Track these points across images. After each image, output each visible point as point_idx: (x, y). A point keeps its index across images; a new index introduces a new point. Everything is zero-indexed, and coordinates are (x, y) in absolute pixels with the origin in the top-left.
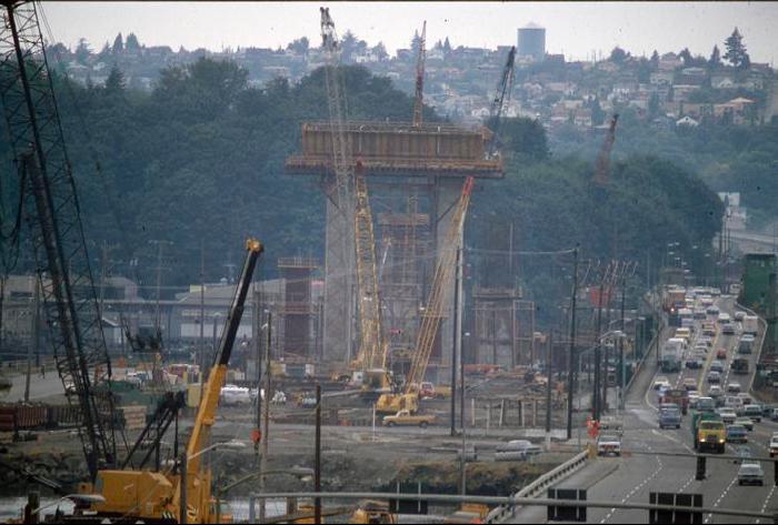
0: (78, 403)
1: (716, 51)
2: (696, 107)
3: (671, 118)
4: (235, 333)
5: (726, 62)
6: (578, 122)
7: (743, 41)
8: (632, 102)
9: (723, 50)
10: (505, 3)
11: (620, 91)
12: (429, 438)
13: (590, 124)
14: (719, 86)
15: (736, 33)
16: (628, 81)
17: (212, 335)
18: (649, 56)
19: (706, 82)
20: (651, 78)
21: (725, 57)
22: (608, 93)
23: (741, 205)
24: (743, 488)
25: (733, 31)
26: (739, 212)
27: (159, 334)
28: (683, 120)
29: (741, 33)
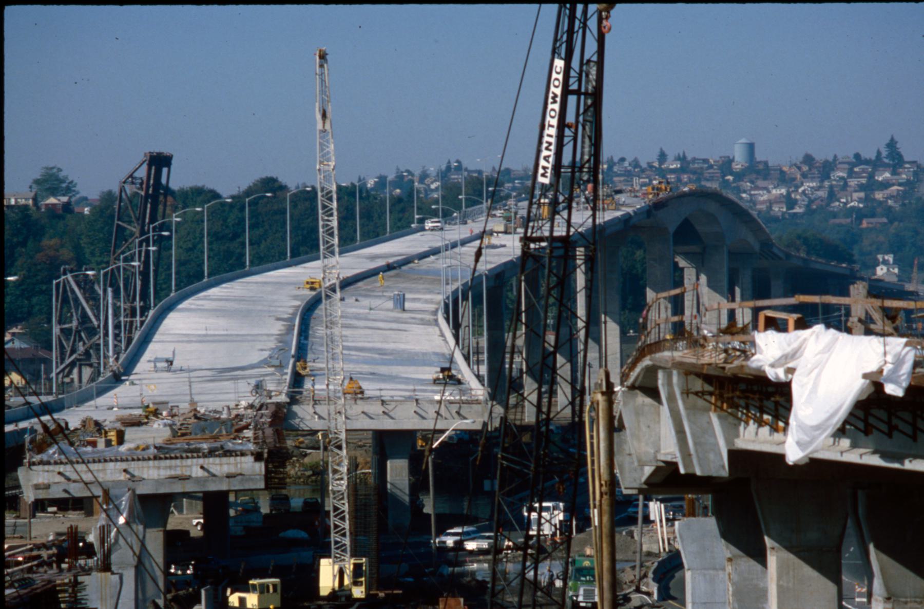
0: (578, 249)
1: (879, 153)
2: (862, 195)
3: (843, 203)
4: (163, 319)
5: (886, 161)
6: (776, 208)
7: (898, 146)
8: (115, 529)
9: (884, 153)
10: (852, 4)
11: (808, 185)
12: (117, 326)
13: (784, 210)
14: (880, 179)
15: (892, 139)
16: (814, 178)
17: (511, 579)
18: (831, 159)
19: (871, 177)
20: (832, 175)
21: (886, 158)
22: (800, 187)
23: (894, 263)
24: (415, 414)
25: (889, 138)
26: (893, 269)
27: (734, 158)
28: (852, 204)
29: (896, 138)
